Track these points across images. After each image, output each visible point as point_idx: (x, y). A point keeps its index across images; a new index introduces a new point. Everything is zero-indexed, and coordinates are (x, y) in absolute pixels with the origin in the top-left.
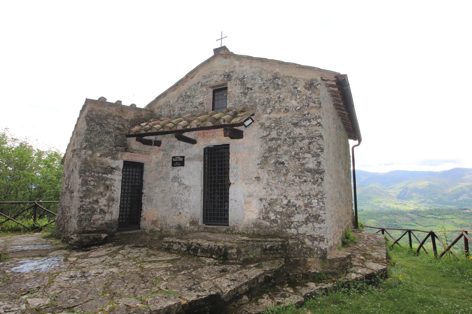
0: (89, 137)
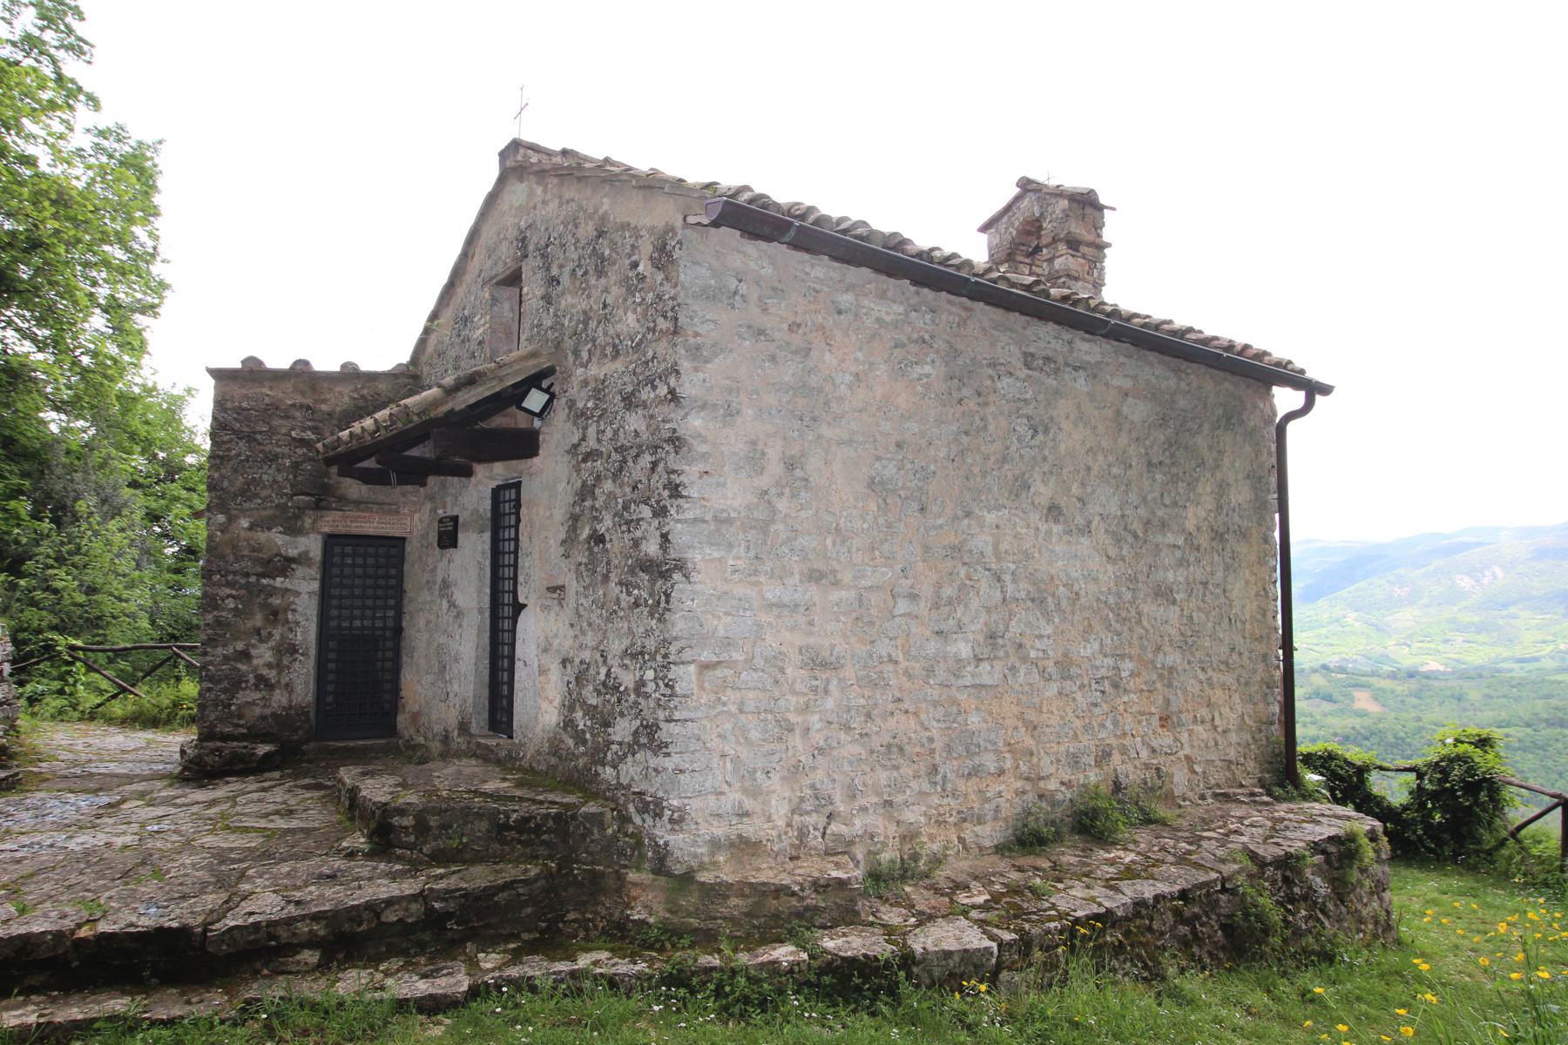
0: (216, 475)
